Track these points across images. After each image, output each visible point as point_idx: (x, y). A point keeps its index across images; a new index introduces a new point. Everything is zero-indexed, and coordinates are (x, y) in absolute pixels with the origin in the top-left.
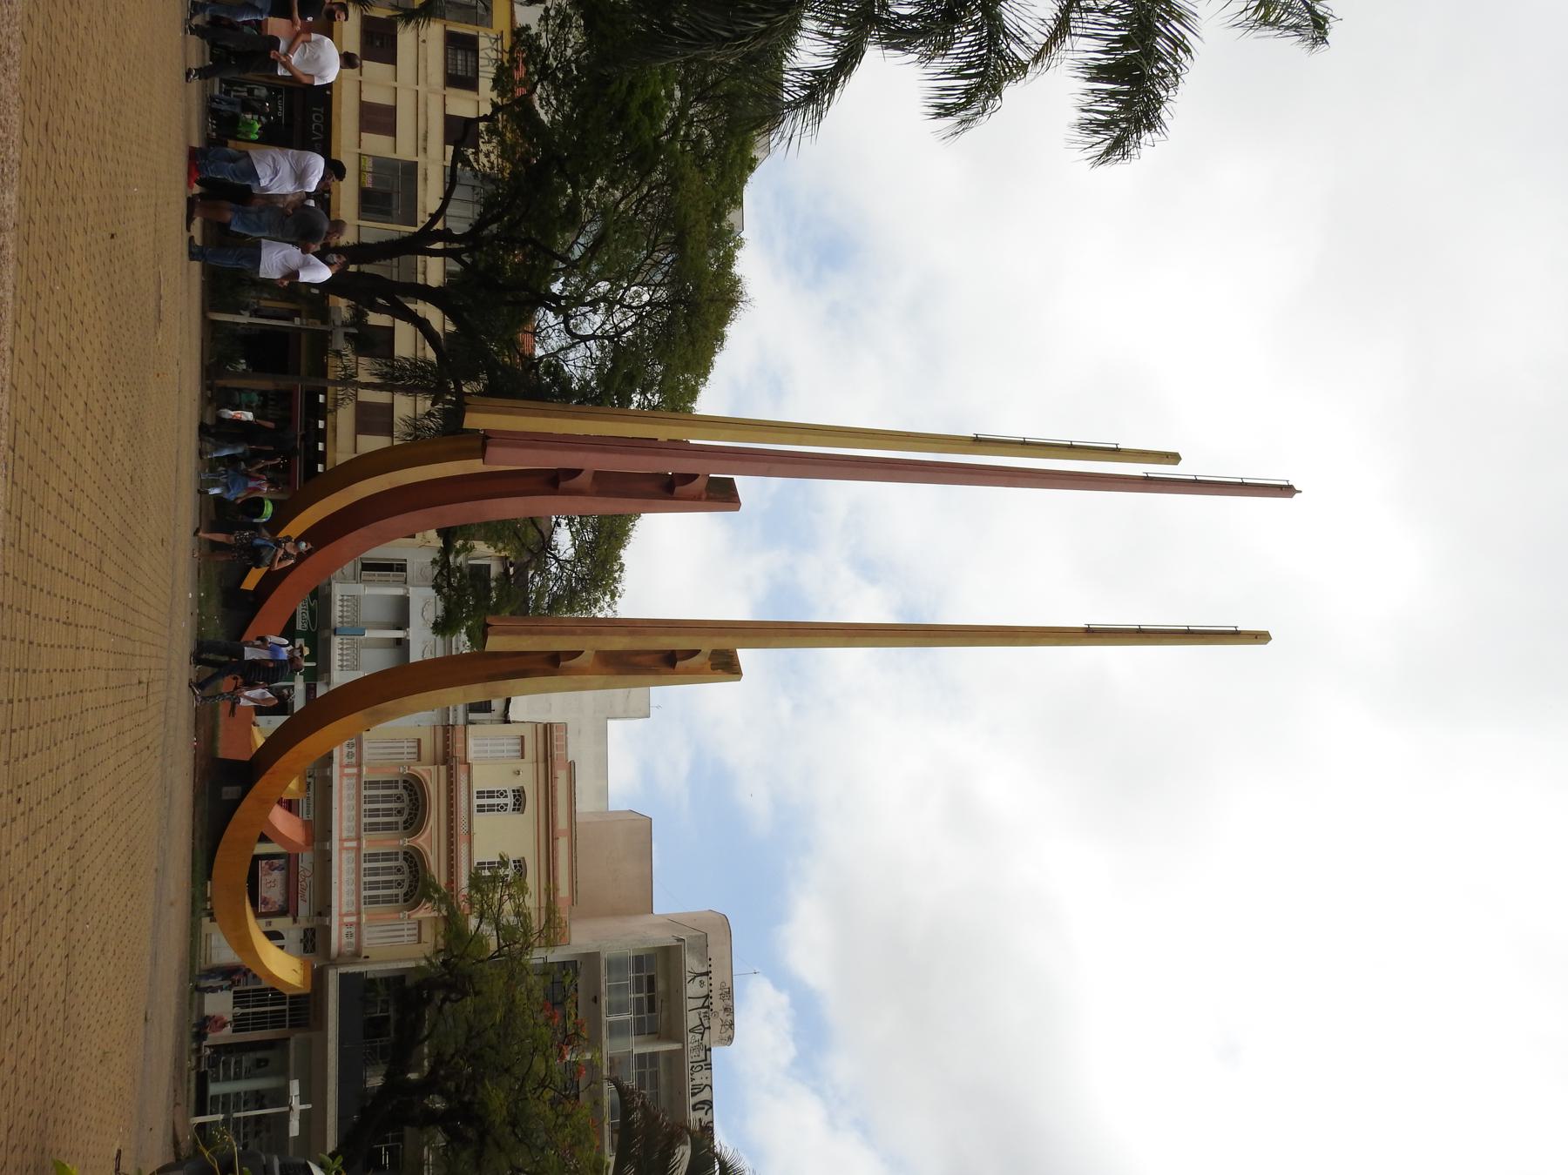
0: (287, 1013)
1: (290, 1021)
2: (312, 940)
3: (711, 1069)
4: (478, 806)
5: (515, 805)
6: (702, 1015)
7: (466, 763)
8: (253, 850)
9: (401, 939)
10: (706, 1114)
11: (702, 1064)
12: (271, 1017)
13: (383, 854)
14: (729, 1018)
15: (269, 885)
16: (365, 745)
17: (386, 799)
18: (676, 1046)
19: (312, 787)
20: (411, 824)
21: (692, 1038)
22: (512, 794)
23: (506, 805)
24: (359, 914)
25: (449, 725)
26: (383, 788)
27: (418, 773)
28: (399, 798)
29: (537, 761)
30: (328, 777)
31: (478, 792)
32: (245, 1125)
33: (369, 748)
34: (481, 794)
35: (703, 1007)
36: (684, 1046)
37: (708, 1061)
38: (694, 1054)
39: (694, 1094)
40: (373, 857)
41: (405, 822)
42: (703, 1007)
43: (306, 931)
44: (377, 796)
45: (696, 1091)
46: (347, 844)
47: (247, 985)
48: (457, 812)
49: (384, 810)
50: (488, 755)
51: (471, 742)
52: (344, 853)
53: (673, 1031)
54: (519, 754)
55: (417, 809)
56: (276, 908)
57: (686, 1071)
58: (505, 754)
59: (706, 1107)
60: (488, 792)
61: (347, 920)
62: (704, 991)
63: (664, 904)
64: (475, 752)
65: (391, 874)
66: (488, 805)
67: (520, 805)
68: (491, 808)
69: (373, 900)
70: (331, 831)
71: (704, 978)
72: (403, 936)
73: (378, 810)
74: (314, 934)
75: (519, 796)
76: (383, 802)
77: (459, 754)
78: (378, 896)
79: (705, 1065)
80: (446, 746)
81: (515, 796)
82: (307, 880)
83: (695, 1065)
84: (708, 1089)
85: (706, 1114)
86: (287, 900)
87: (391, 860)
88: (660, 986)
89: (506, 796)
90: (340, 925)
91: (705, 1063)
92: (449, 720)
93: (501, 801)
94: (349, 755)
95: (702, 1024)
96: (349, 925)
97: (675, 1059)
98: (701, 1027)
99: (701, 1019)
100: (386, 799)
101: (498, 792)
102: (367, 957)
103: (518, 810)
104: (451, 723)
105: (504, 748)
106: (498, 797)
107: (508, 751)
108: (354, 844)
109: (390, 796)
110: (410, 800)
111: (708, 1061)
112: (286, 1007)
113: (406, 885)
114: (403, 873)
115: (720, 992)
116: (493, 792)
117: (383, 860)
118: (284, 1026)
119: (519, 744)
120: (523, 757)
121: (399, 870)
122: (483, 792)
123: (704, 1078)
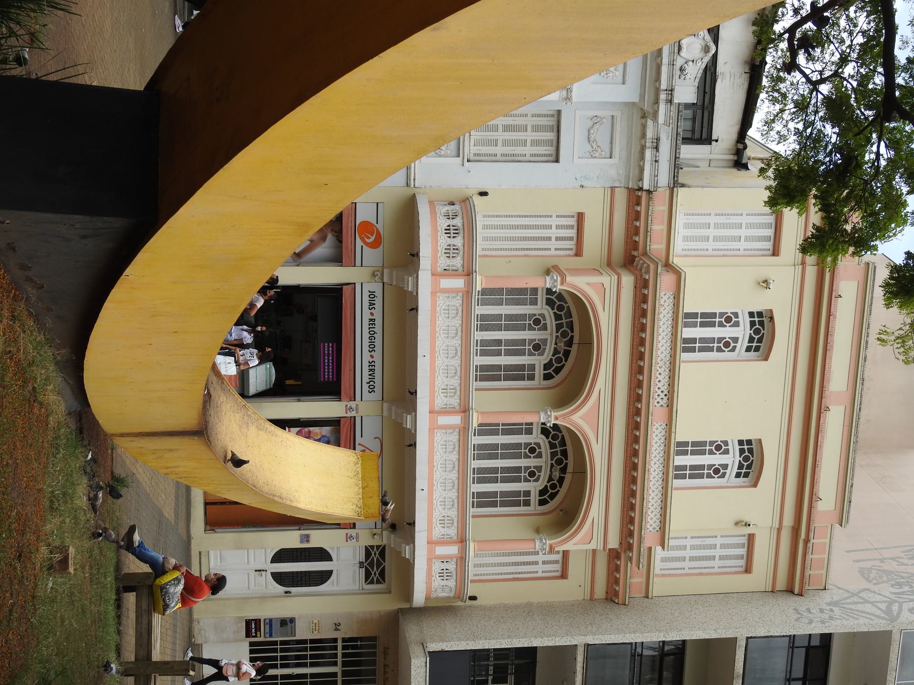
1: (344, 655)
2: (379, 564)
5: (751, 340)
7: (668, 265)
8: (275, 270)
9: (544, 244)
17: (514, 322)
19: (378, 302)
20: (558, 371)
22: (737, 448)
23: (736, 340)
24: (462, 540)
25: (641, 189)
26: (509, 302)
27: (579, 290)
28: (537, 322)
29: (779, 530)
30: (410, 430)
41: (547, 366)
43: (368, 551)
44: (499, 317)
46: (443, 420)
47: (271, 636)
48: (646, 231)
49: (509, 342)
50: (711, 245)
51: (680, 220)
52: (439, 437)
54: (769, 245)
58: (743, 245)
60: (694, 444)
61: (441, 550)
64: (686, 239)
65: (517, 456)
66: (702, 340)
70: (414, 393)
72: (536, 563)
73: (498, 342)
75: (762, 323)
76: (508, 328)
77: (656, 247)
80: (632, 230)
81: (752, 324)
89: (737, 324)
92: (641, 179)
93: (727, 332)
94: (450, 251)
96: (444, 559)
100: (514, 322)
101: (711, 443)
102: (473, 598)
103: (757, 349)
104: (646, 187)
105: (743, 232)
106: (711, 453)
107: (748, 239)
108: (456, 420)
109: (523, 317)
112: (337, 669)
113: (544, 476)
114: (540, 456)
116: (713, 315)
119: (767, 226)
120: (775, 252)
121: (532, 450)
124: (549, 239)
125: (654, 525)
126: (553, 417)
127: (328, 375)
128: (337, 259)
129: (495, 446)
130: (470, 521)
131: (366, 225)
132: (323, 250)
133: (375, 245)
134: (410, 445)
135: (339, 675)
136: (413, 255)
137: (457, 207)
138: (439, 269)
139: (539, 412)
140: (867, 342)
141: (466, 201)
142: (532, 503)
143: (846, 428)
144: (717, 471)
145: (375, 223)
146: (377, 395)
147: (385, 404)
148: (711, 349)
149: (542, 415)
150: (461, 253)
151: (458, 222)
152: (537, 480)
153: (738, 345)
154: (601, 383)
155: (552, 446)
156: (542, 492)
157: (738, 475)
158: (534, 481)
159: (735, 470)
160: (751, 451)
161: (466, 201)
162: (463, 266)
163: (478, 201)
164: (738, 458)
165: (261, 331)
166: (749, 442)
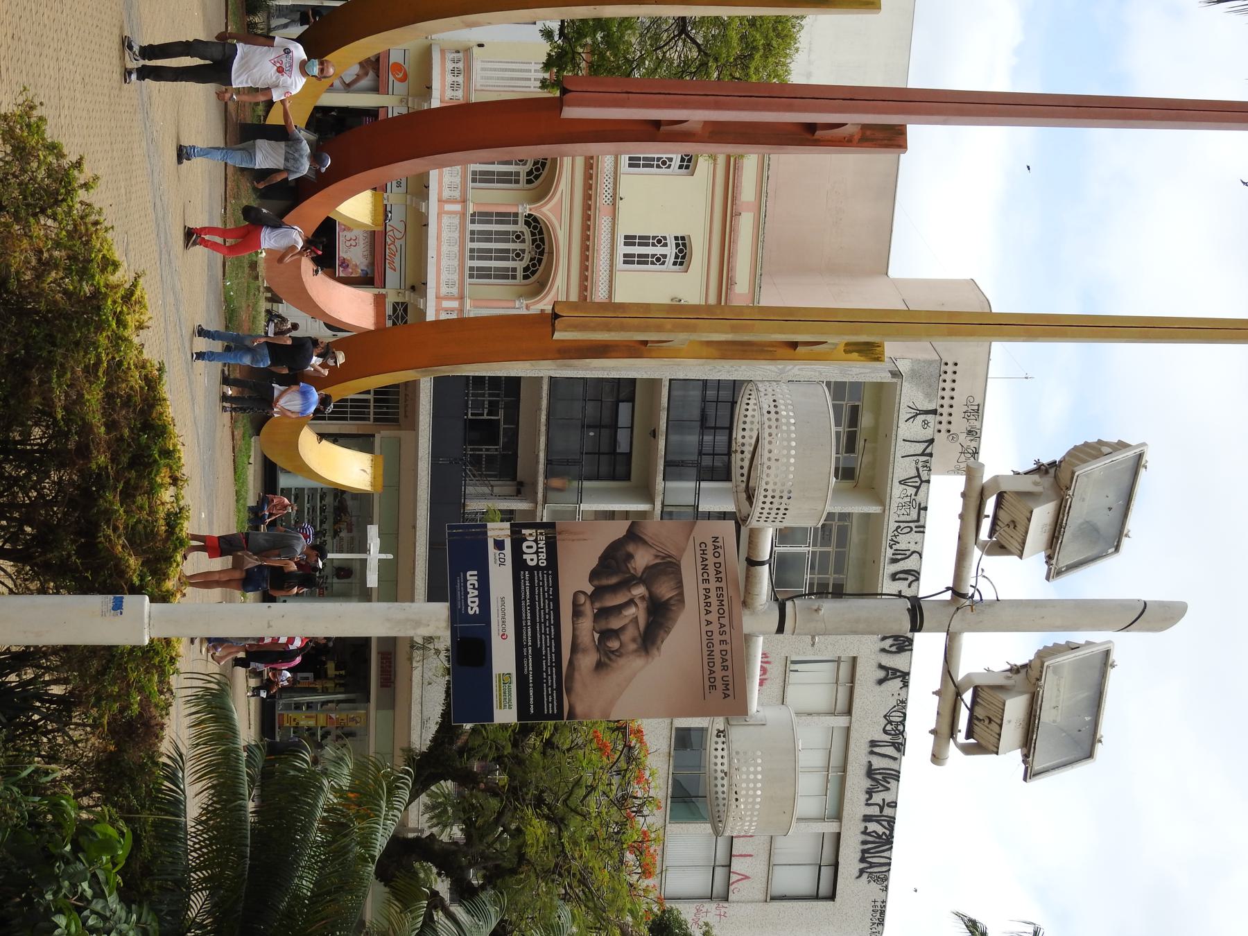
0: (372, 404)
1: (375, 413)
2: (403, 318)
3: (924, 532)
4: (625, 256)
5: (677, 257)
6: (920, 464)
10: (909, 586)
11: (912, 525)
12: (351, 407)
13: (498, 214)
14: (973, 444)
15: (348, 244)
16: (477, 66)
18: (874, 509)
21: (897, 492)
23: (665, 256)
28: (518, 237)
31: (626, 237)
32: (322, 498)
33: (482, 69)
34: (630, 240)
35: (923, 454)
36: (884, 511)
37: (921, 523)
38: (903, 511)
39: (894, 561)
40: (484, 217)
42: (923, 454)
45: (899, 557)
46: (448, 207)
52: (446, 220)
53: (875, 490)
55: (542, 253)
56: (358, 273)
57: (884, 542)
59: (911, 578)
60: (641, 238)
61: (446, 304)
62: (928, 433)
63: (897, 269)
65: (507, 241)
66: (639, 256)
67: (683, 257)
68: (643, 259)
69: (483, 273)
71: (930, 417)
74: (405, 310)
78: (489, 269)
79: (916, 527)
81: (677, 245)
82: (398, 243)
83: (902, 525)
84: (915, 556)
85: (909, 586)
86: (372, 264)
87: (508, 223)
88: (866, 420)
89: (666, 245)
90: (439, 215)
91: (916, 524)
93: (658, 250)
95: (919, 476)
97: (871, 523)
98: (917, 479)
99: (918, 469)
100: (503, 236)
101: (654, 238)
106: (654, 245)
108: (458, 207)
110: (534, 241)
111: (921, 523)
113: (527, 257)
114: (523, 241)
115: (965, 408)
117: (498, 222)
118: (368, 419)
121: (518, 237)
122: (634, 237)
123: (913, 543)
124: (530, 79)
125: (604, 294)
126: (525, 209)
127: (548, 710)
128: (375, 89)
129: (490, 233)
130: (467, 287)
131: (396, 64)
132: (365, 82)
133: (403, 80)
134: (425, 225)
135: (372, 401)
136: (428, 88)
137: (461, 55)
138: (446, 98)
139: (517, 205)
140: (769, 165)
141: (468, 50)
142: (518, 277)
143: (755, 231)
144: (658, 260)
145: (403, 64)
146: (403, 189)
147: (408, 196)
148: (652, 166)
149: (520, 207)
150: (462, 87)
151: (461, 65)
152: (521, 260)
153: (673, 163)
154: (563, 185)
155: (533, 234)
156: (526, 269)
157: (675, 263)
158: (520, 260)
159: (673, 260)
160: (684, 245)
161: (468, 50)
162: (463, 97)
163: (476, 50)
164: (674, 251)
165: (9, 663)
166: (683, 238)
